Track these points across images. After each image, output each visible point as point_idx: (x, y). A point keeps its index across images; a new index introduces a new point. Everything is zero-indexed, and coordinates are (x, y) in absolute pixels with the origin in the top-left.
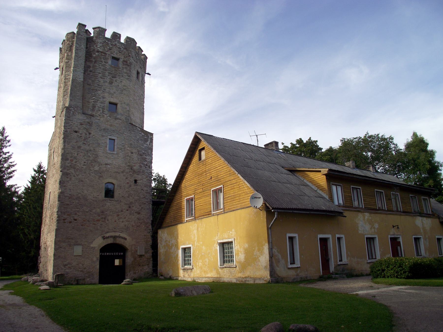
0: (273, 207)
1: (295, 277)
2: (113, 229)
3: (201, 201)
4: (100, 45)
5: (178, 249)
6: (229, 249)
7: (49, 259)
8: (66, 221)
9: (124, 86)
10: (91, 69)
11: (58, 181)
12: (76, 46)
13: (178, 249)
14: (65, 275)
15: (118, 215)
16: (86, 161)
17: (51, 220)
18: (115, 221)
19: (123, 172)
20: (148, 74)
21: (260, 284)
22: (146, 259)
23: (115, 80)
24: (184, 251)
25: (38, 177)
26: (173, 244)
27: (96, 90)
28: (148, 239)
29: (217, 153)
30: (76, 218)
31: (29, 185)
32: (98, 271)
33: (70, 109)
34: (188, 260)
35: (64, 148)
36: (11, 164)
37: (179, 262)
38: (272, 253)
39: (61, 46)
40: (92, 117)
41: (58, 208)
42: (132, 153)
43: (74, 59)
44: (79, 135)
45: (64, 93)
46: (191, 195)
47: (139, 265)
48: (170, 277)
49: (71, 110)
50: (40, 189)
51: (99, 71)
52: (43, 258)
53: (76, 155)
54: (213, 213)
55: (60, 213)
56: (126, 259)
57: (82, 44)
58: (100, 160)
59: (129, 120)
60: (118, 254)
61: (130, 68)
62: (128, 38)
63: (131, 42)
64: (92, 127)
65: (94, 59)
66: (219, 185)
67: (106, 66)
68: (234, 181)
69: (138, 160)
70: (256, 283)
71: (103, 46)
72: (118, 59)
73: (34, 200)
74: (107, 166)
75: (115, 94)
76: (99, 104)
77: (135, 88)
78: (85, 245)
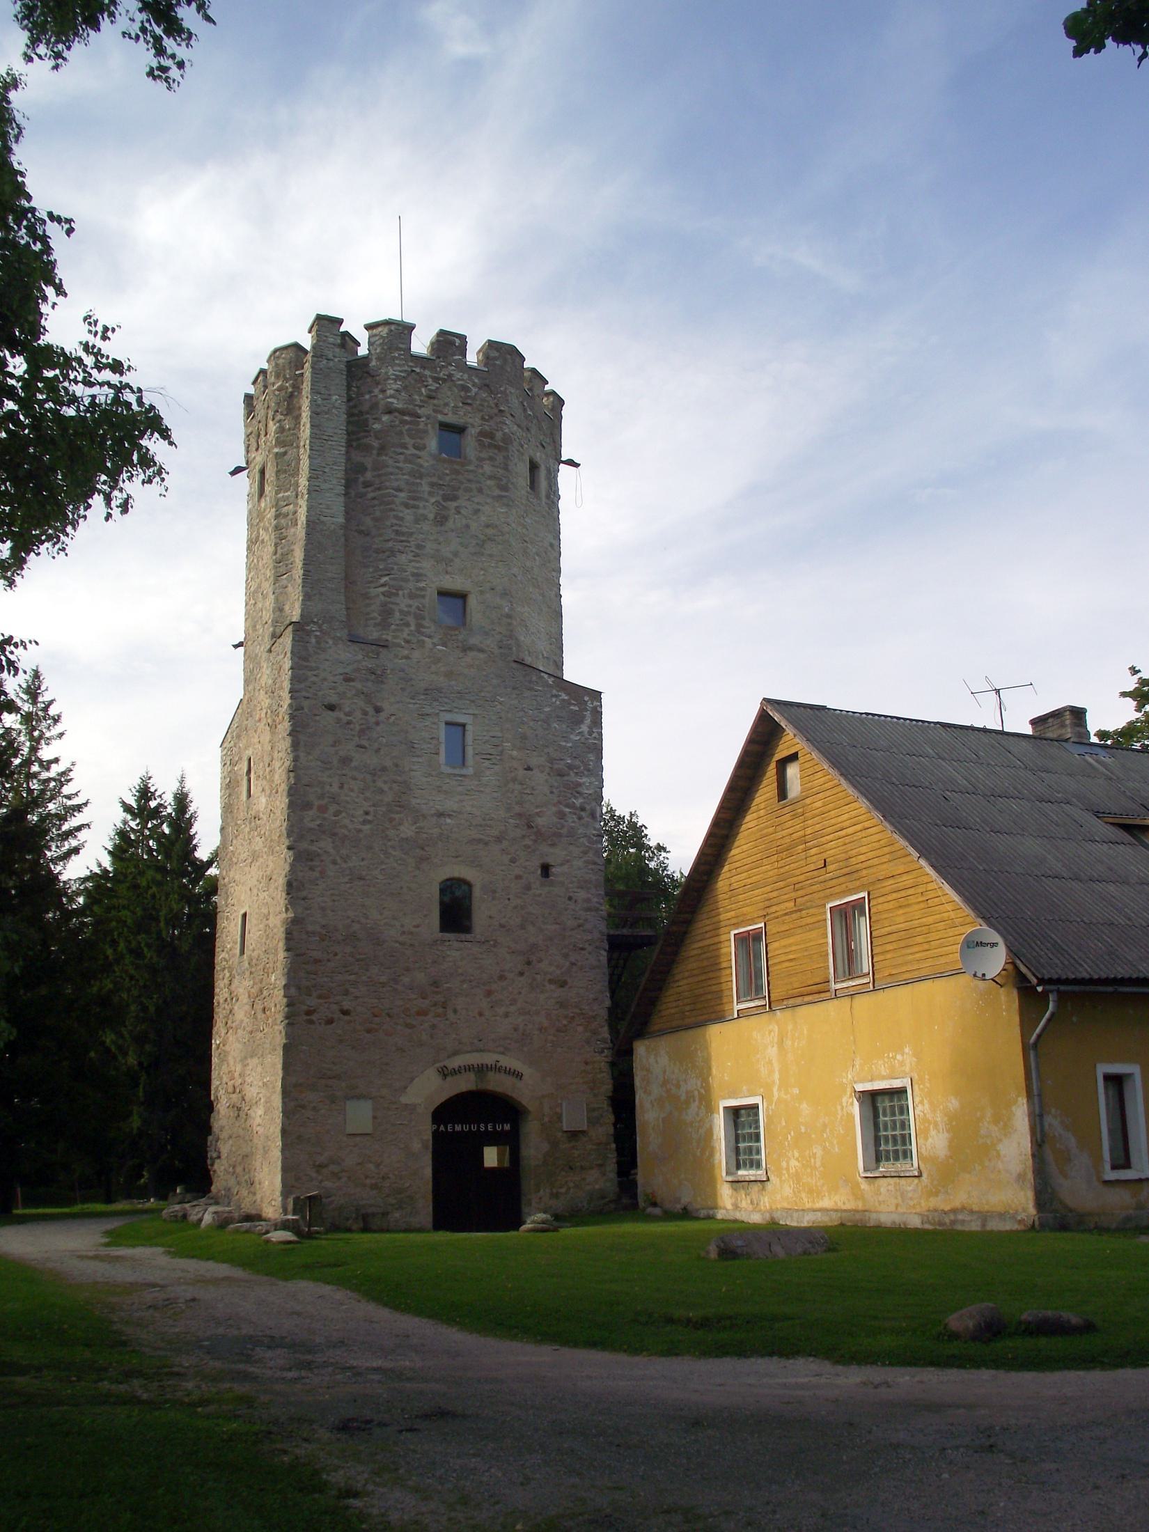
0: (1040, 976)
1: (1131, 1211)
2: (476, 1041)
3: (790, 945)
4: (395, 387)
5: (710, 1109)
6: (893, 1114)
7: (260, 1147)
8: (314, 1017)
9: (488, 526)
10: (369, 475)
11: (280, 881)
12: (313, 402)
13: (712, 1113)
14: (324, 1200)
15: (489, 993)
16: (371, 809)
17: (260, 1015)
18: (481, 1014)
19: (499, 839)
20: (571, 463)
21: (1000, 1232)
22: (594, 1147)
23: (457, 507)
24: (732, 1116)
25: (141, 831)
26: (693, 1092)
27: (392, 552)
28: (599, 1076)
29: (843, 781)
30: (346, 1005)
31: (107, 862)
32: (430, 1186)
33: (309, 628)
34: (750, 1150)
35: (295, 766)
36: (69, 803)
37: (717, 1156)
38: (1042, 1130)
39: (251, 390)
40: (383, 651)
41: (288, 973)
42: (529, 769)
43: (310, 450)
44: (342, 715)
45: (275, 567)
46: (753, 922)
47: (571, 1168)
48: (685, 1209)
49: (309, 633)
50: (154, 880)
51: (397, 480)
52: (231, 1142)
53: (335, 789)
54: (833, 986)
55: (293, 991)
56: (523, 1146)
57: (332, 392)
58: (418, 801)
59: (511, 649)
60: (494, 1127)
61: (506, 458)
62: (492, 345)
63: (505, 360)
64: (383, 686)
65: (377, 438)
66: (856, 891)
67: (419, 460)
68: (907, 880)
69: (552, 792)
70: (988, 1228)
71: (405, 388)
72: (460, 430)
73: (129, 921)
74: (442, 820)
75: (457, 560)
76: (403, 602)
77: (524, 526)
78: (382, 1097)
